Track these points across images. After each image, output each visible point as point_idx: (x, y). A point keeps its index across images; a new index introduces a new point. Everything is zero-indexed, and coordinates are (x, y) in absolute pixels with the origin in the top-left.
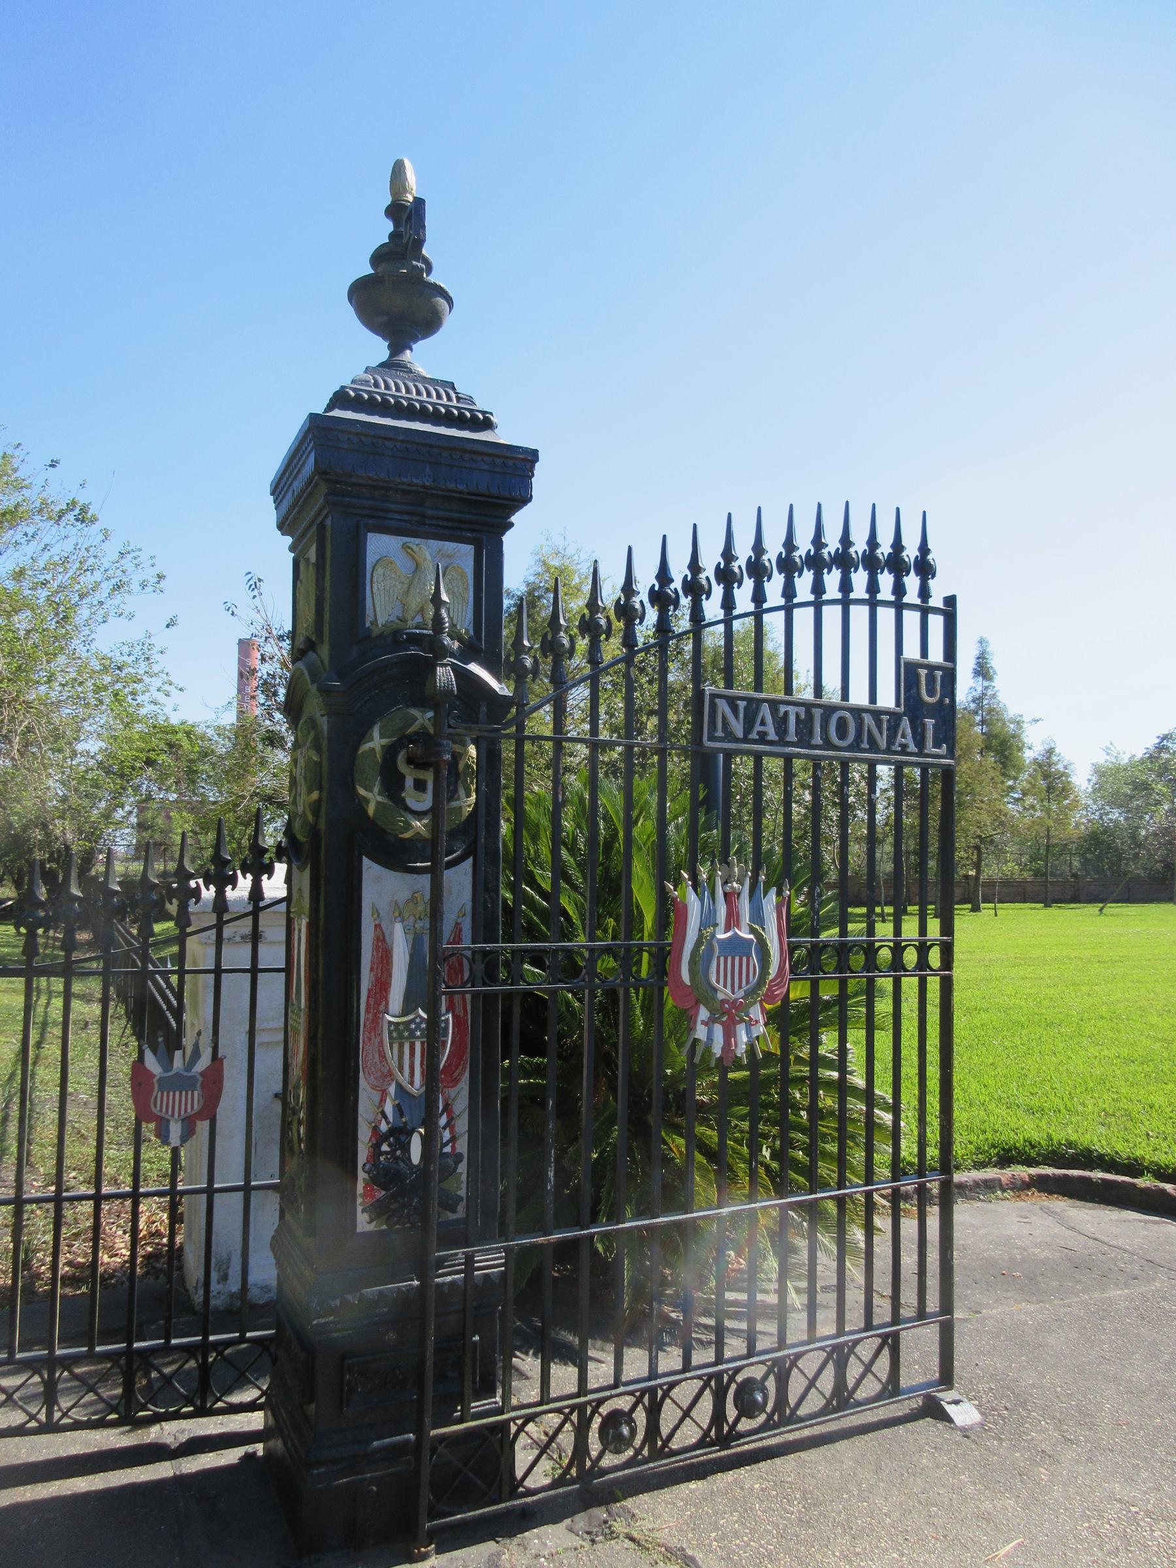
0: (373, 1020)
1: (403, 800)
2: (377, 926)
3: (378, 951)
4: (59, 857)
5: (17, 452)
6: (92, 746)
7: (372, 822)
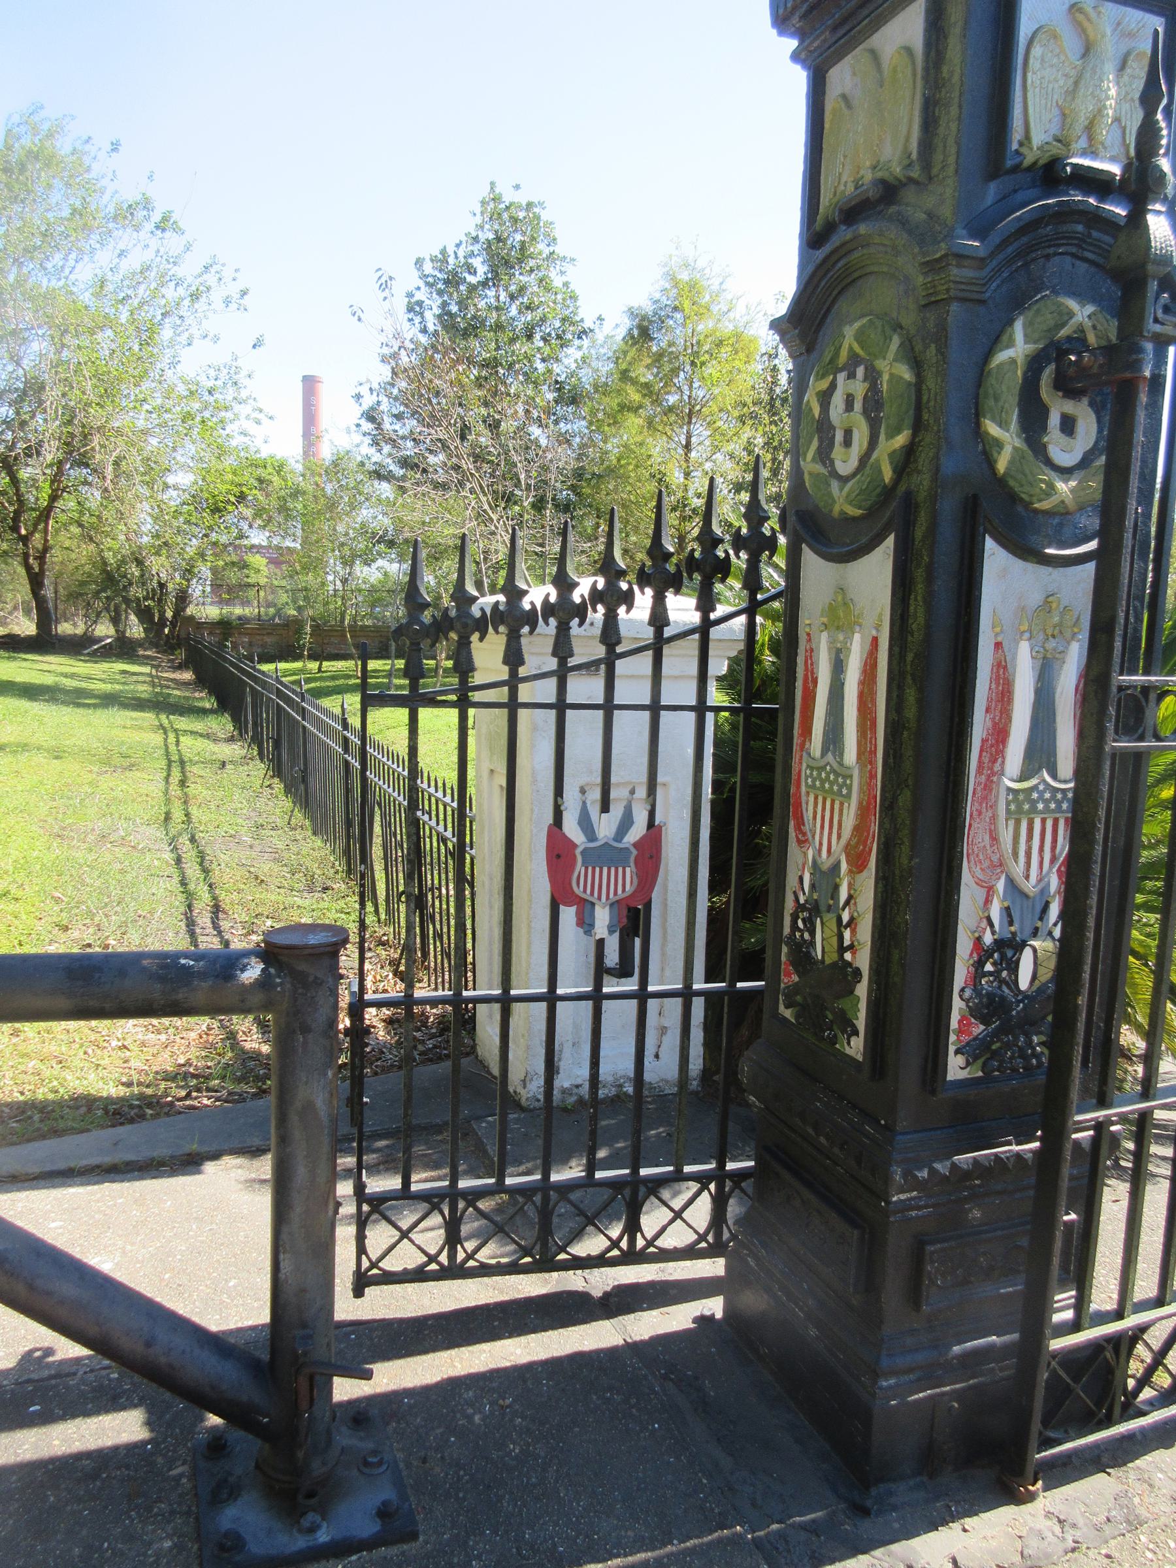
0: (986, 785)
1: (1045, 446)
2: (998, 645)
3: (998, 684)
4: (154, 595)
5: (87, 147)
6: (183, 479)
7: (1001, 482)
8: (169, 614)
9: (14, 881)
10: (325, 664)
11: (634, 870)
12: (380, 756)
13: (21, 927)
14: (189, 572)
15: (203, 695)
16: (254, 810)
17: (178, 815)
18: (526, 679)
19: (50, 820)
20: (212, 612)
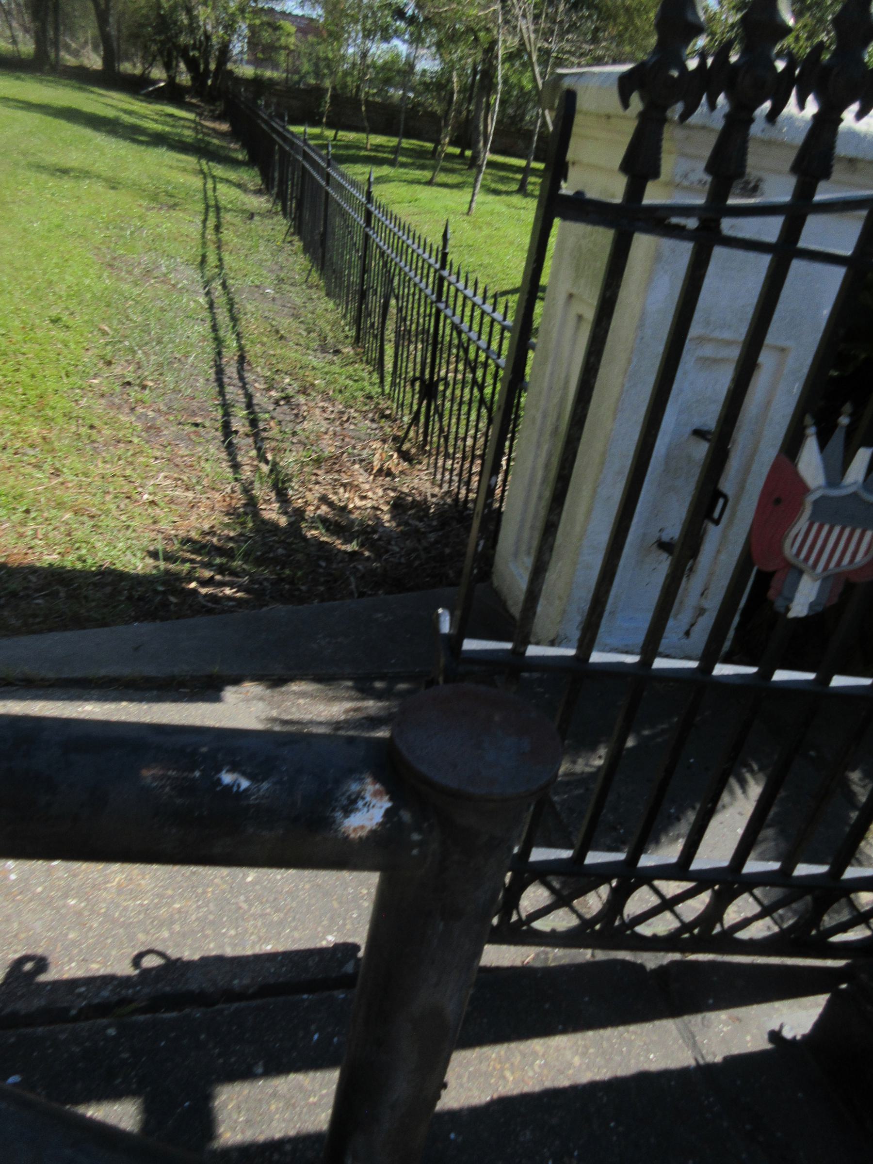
8: (213, 66)
9: (67, 308)
10: (340, 133)
13: (69, 356)
14: (230, 28)
15: (237, 146)
16: (277, 263)
17: (212, 259)
19: (104, 249)
20: (247, 71)
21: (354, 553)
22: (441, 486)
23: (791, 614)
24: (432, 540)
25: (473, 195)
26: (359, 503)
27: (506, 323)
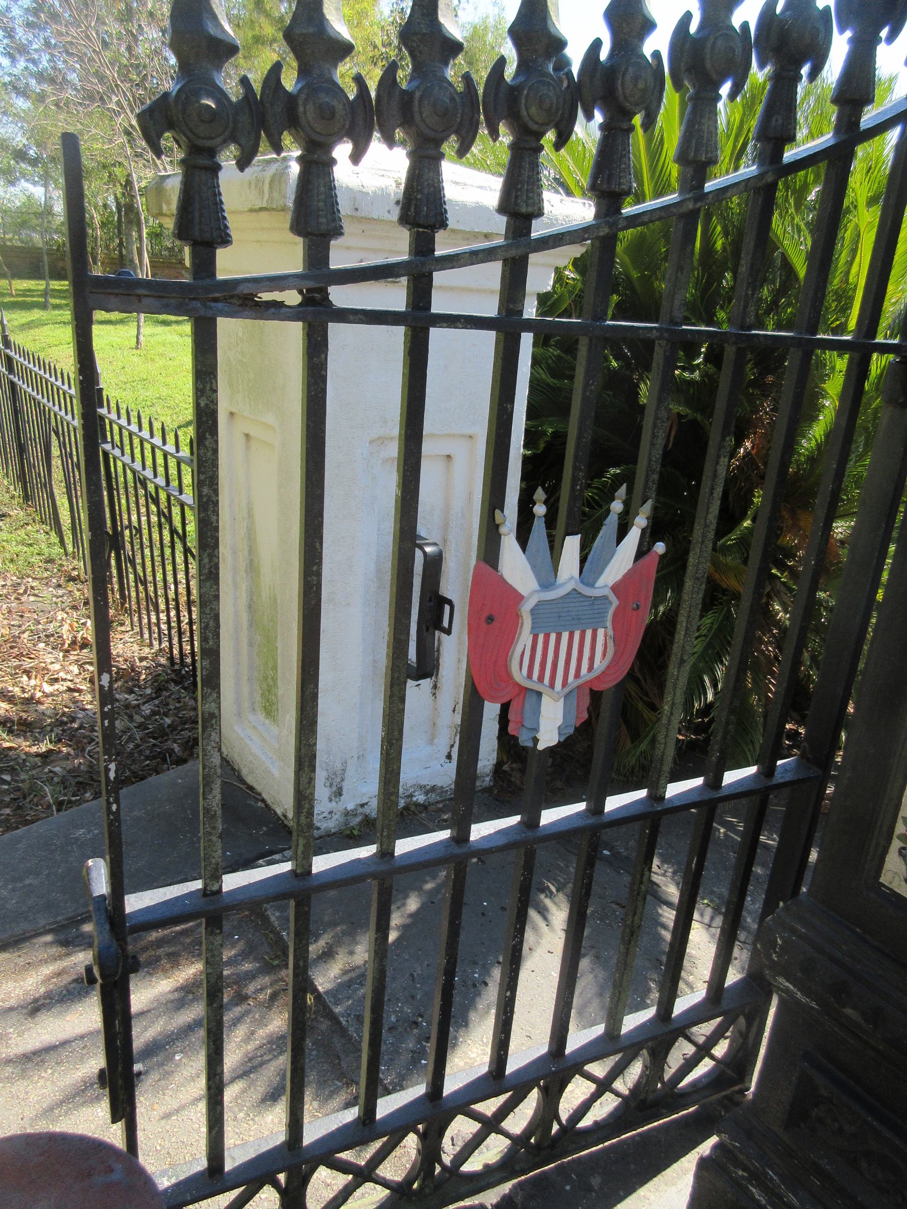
11: (610, 632)
12: (53, 379)
18: (452, 261)
21: (46, 757)
22: (151, 645)
23: (541, 747)
24: (148, 712)
25: (139, 327)
26: (48, 689)
27: (181, 454)
